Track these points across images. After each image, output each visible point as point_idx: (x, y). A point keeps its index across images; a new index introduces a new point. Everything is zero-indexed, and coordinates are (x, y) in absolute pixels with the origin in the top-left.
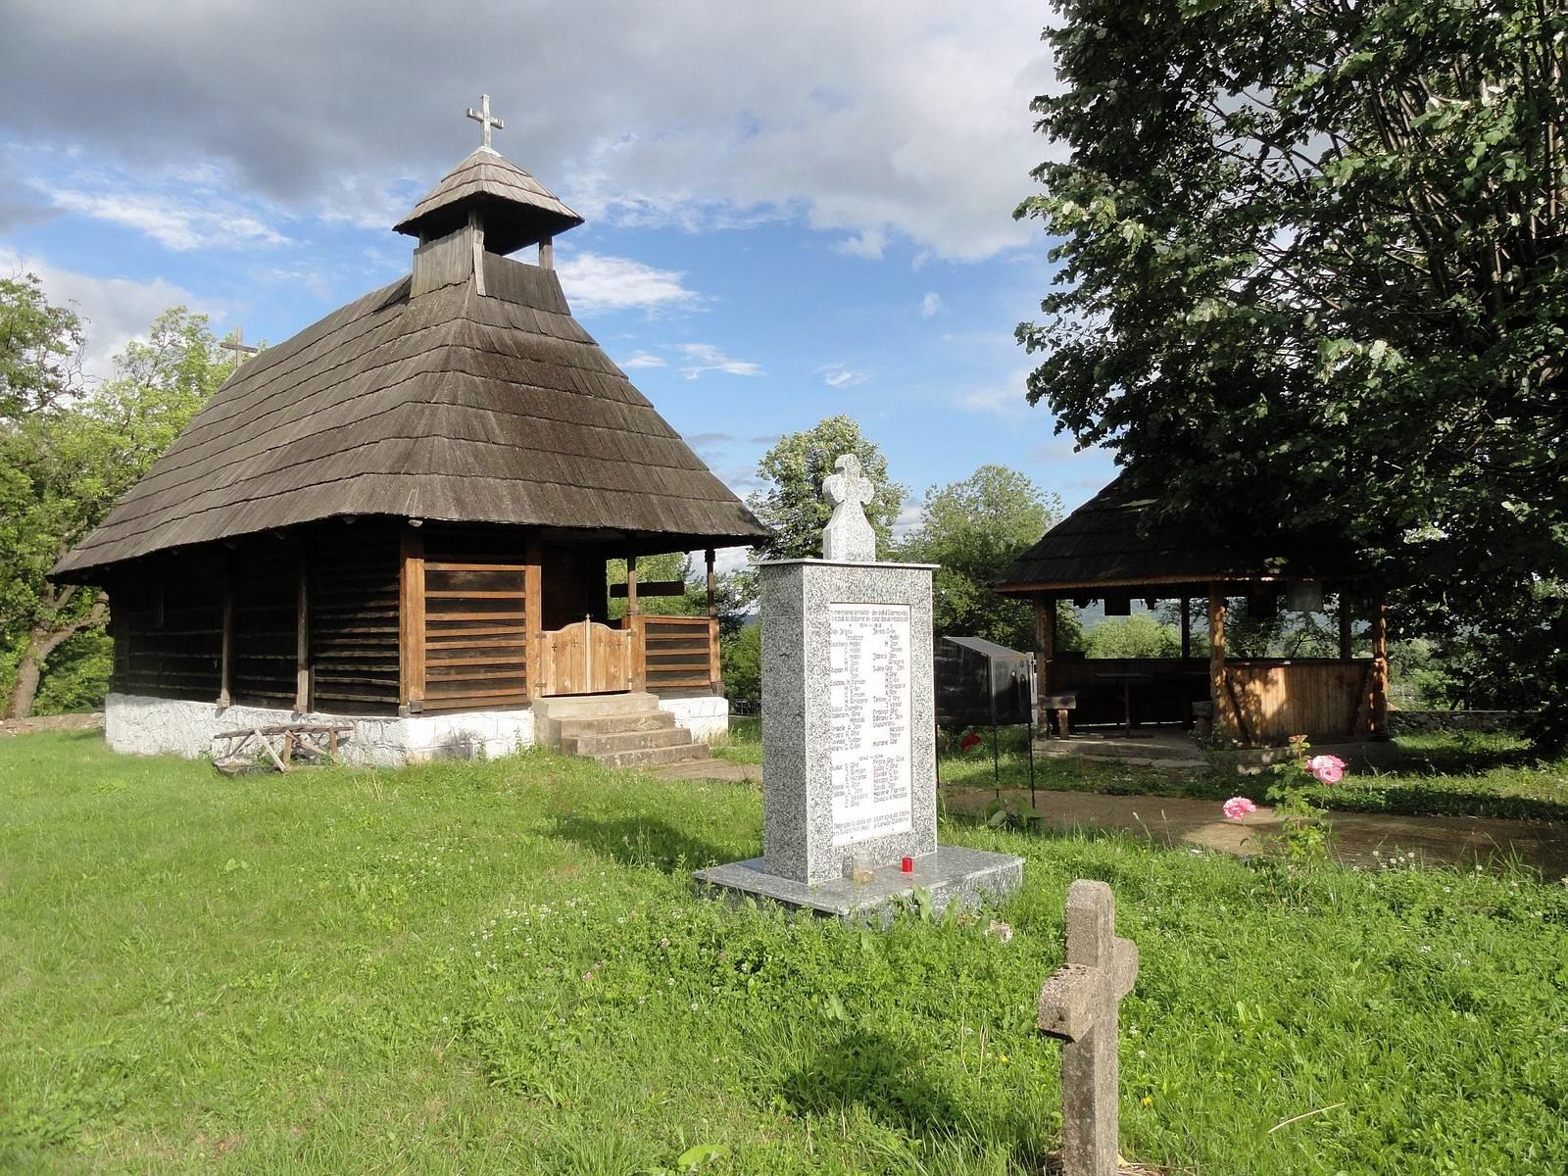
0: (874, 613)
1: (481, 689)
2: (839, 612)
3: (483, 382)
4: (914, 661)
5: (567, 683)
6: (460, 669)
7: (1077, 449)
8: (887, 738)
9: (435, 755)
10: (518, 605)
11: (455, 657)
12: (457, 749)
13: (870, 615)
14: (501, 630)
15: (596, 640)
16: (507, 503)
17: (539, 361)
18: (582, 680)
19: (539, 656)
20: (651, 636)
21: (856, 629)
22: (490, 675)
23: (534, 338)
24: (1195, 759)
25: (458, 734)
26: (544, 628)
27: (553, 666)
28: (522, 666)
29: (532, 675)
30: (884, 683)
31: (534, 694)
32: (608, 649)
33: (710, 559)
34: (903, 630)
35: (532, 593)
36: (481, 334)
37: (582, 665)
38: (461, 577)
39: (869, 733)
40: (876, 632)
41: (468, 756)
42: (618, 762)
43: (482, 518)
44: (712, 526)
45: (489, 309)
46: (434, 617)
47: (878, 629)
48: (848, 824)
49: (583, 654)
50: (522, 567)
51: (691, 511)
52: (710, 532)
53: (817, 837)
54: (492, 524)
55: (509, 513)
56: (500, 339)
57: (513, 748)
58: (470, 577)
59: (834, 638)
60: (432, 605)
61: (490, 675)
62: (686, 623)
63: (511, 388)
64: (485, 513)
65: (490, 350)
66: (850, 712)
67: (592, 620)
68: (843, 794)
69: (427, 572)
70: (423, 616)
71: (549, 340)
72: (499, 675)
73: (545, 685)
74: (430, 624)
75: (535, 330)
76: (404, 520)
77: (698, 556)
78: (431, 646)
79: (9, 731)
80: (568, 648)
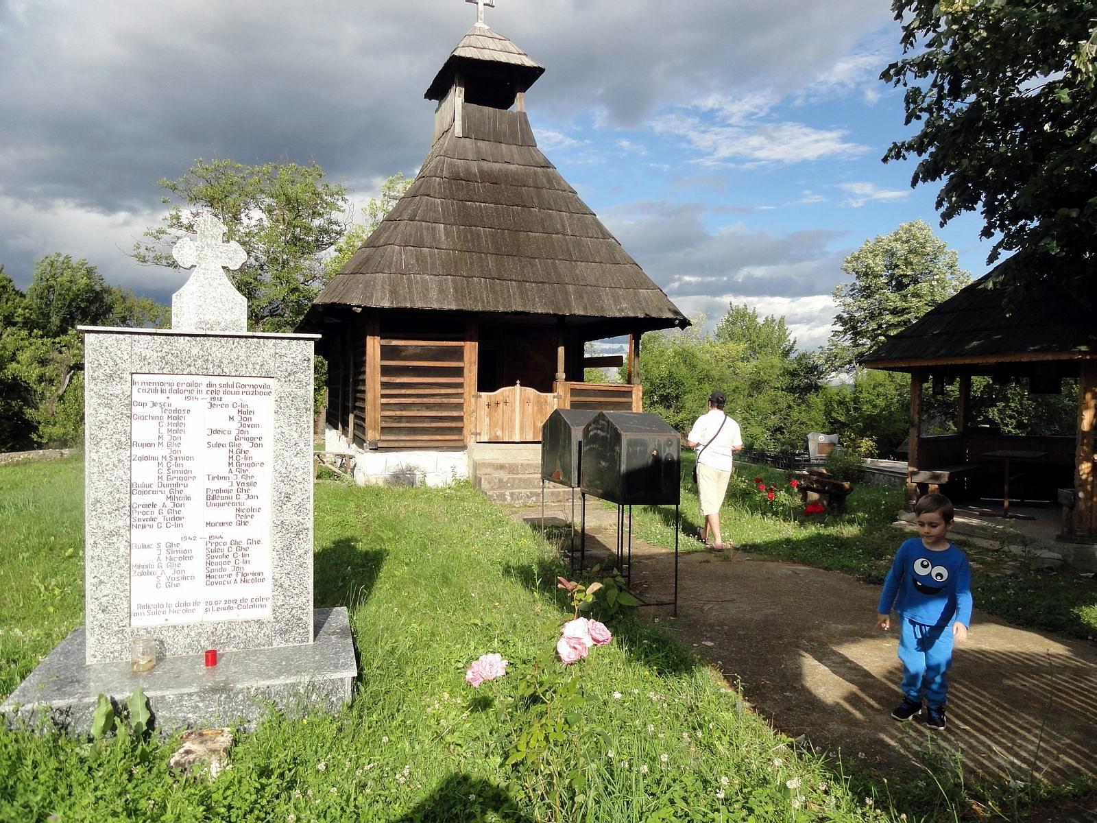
0: (209, 385)
1: (425, 434)
2: (149, 384)
3: (442, 203)
4: (281, 438)
5: (499, 433)
6: (410, 419)
7: (942, 225)
9: (386, 481)
10: (459, 372)
11: (405, 410)
12: (403, 479)
13: (204, 388)
14: (443, 391)
15: (525, 401)
16: (434, 294)
17: (496, 183)
18: (512, 432)
19: (474, 411)
20: (576, 399)
21: (178, 401)
22: (434, 425)
23: (497, 166)
24: (1049, 550)
25: (404, 467)
27: (487, 420)
28: (460, 419)
29: (468, 425)
31: (470, 441)
32: (536, 408)
34: (263, 408)
35: (470, 363)
36: (452, 166)
37: (512, 420)
38: (411, 351)
39: (196, 513)
40: (212, 406)
41: (412, 483)
42: (509, 498)
43: (409, 306)
44: (621, 310)
45: (464, 147)
46: (385, 379)
47: (217, 402)
48: (159, 606)
49: (513, 411)
50: (462, 343)
52: (617, 315)
53: (101, 616)
55: (433, 302)
56: (468, 171)
57: (449, 480)
58: (418, 350)
59: (136, 410)
60: (385, 371)
61: (434, 425)
62: (611, 389)
63: (464, 207)
64: (412, 301)
65: (456, 178)
66: (167, 490)
67: (522, 385)
68: (152, 574)
69: (382, 347)
70: (379, 378)
71: (512, 167)
72: (440, 425)
73: (480, 434)
74: (385, 385)
76: (348, 308)
78: (384, 401)
80: (500, 406)
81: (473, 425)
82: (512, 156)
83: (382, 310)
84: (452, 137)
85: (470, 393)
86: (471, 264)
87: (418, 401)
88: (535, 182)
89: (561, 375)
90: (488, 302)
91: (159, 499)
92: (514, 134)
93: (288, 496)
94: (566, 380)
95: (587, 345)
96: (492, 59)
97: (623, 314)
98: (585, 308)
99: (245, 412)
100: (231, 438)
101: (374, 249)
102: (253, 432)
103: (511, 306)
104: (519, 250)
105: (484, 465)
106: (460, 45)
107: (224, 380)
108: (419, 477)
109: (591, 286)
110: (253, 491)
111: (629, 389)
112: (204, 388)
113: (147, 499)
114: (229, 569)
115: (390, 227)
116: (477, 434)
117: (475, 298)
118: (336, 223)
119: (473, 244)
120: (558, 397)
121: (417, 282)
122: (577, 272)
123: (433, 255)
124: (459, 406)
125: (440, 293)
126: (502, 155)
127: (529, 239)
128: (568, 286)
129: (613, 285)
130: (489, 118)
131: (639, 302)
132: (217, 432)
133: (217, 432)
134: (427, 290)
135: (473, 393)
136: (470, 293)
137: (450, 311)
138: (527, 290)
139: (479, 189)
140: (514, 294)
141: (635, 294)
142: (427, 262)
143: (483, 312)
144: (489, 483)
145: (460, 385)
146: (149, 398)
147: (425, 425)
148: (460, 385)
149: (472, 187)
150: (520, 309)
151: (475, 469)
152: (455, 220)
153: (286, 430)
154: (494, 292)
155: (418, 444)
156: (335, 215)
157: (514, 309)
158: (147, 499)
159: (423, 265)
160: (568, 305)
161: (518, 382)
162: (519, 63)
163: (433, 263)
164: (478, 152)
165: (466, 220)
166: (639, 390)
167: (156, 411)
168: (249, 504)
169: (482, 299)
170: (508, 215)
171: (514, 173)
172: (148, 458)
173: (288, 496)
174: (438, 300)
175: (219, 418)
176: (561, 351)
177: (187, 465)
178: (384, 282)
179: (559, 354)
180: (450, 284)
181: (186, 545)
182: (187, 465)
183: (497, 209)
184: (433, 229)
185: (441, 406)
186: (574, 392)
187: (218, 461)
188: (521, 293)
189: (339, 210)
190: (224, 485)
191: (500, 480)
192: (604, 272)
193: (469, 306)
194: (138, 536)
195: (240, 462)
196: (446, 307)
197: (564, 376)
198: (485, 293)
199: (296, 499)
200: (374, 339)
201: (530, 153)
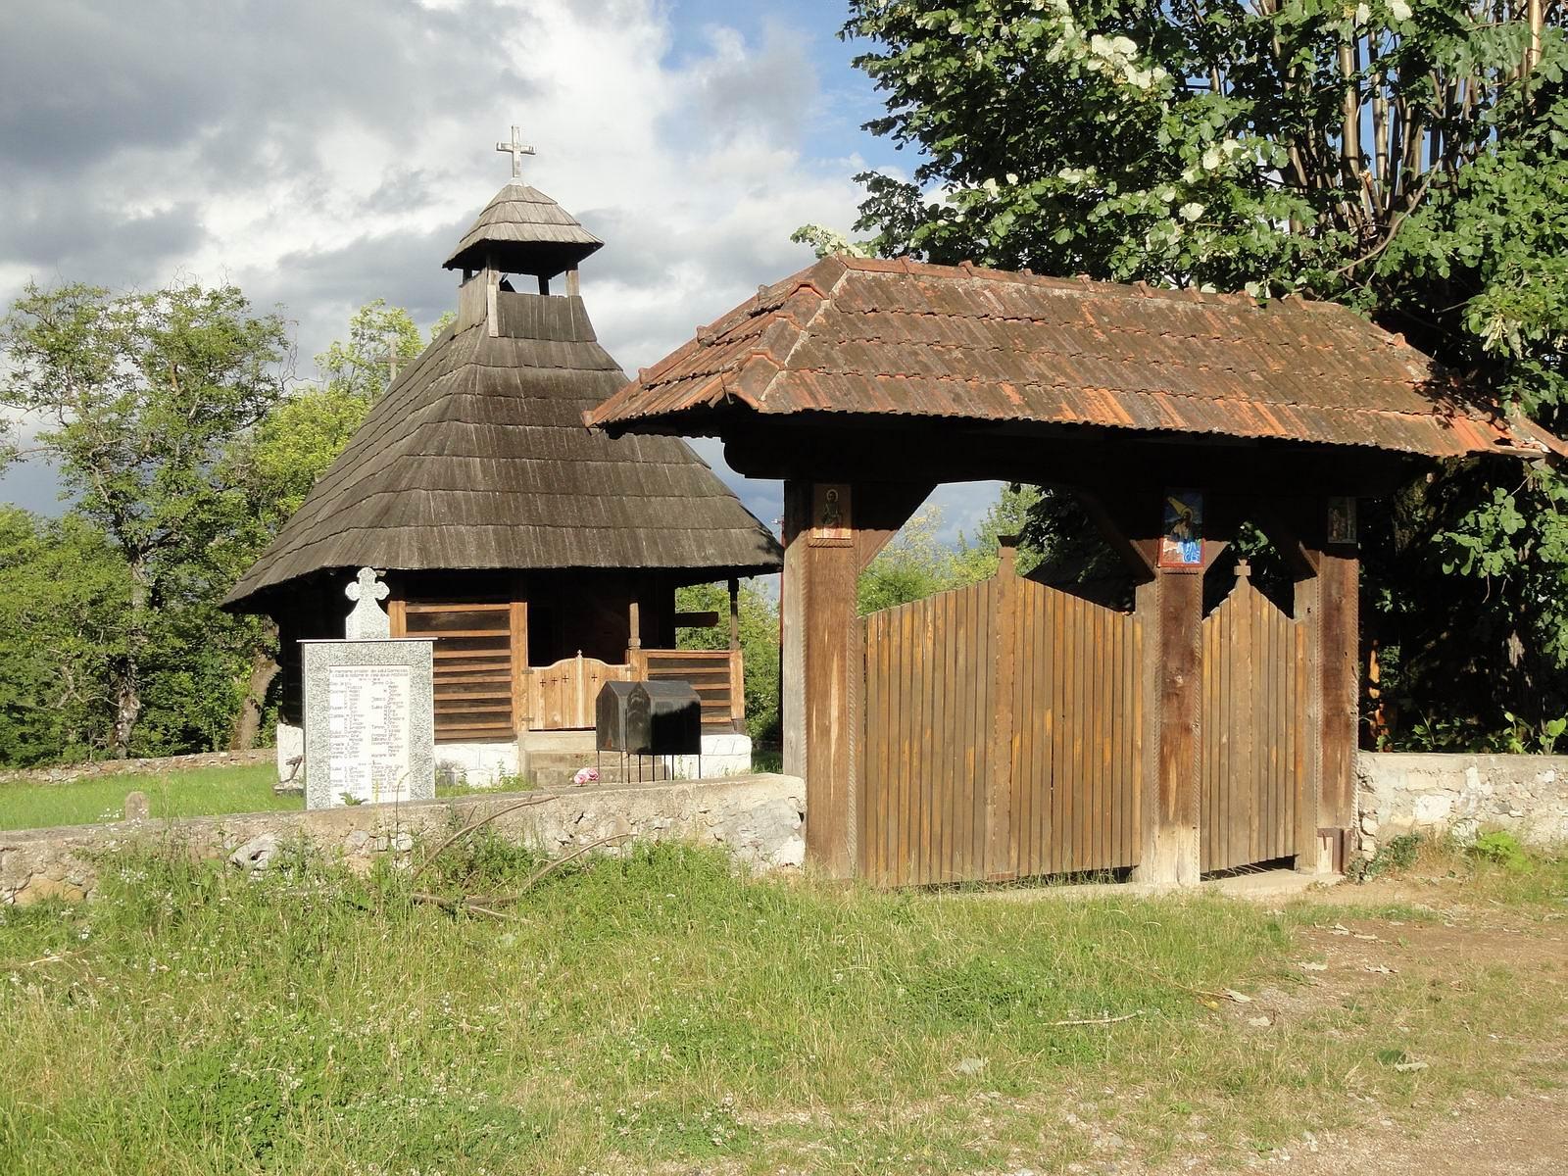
1: (464, 722)
3: (476, 429)
4: (415, 703)
5: (558, 718)
8: (387, 752)
10: (503, 643)
13: (369, 673)
14: (485, 667)
21: (355, 681)
22: (474, 710)
23: (546, 372)
25: (439, 763)
26: (531, 664)
27: (542, 702)
28: (507, 701)
29: (518, 709)
30: (383, 716)
31: (521, 729)
33: (734, 589)
34: (403, 683)
36: (486, 376)
37: (573, 701)
38: (443, 619)
39: (367, 749)
43: (442, 566)
44: (705, 558)
49: (575, 689)
50: (506, 606)
51: (684, 542)
52: (701, 564)
54: (453, 570)
56: (508, 385)
57: (496, 779)
58: (452, 618)
59: (332, 688)
61: (474, 710)
63: (505, 433)
64: (446, 560)
65: (491, 392)
71: (565, 373)
72: (483, 709)
73: (533, 720)
75: (560, 366)
77: (721, 587)
79: (233, 763)
80: (558, 683)
81: (523, 708)
82: (564, 357)
83: (411, 572)
84: (485, 336)
85: (519, 667)
86: (517, 508)
87: (454, 680)
88: (595, 390)
89: (635, 641)
90: (539, 556)
91: (345, 740)
92: (566, 325)
93: (419, 738)
94: (642, 647)
95: (679, 591)
96: (535, 239)
97: (709, 563)
98: (660, 558)
99: (393, 687)
100: (386, 703)
101: (395, 495)
102: (397, 699)
103: (566, 560)
104: (575, 485)
105: (541, 756)
106: (493, 221)
107: (380, 668)
108: (457, 775)
109: (668, 528)
110: (399, 735)
111: (726, 656)
112: (369, 673)
113: (338, 741)
114: (385, 784)
115: (412, 465)
116: (529, 720)
117: (523, 551)
118: (268, 381)
119: (518, 483)
120: (632, 669)
121: (451, 536)
122: (651, 511)
123: (468, 501)
124: (506, 686)
125: (479, 548)
126: (551, 356)
127: (588, 471)
128: (638, 531)
129: (697, 526)
130: (533, 308)
131: (730, 545)
132: (377, 699)
133: (377, 699)
134: (463, 544)
135: (522, 668)
136: (516, 546)
137: (492, 571)
138: (586, 538)
139: (522, 408)
140: (571, 544)
141: (725, 535)
142: (461, 510)
143: (533, 569)
144: (546, 777)
145: (507, 659)
146: (339, 680)
147: (464, 710)
148: (507, 659)
149: (513, 405)
150: (578, 563)
151: (528, 764)
152: (494, 452)
153: (417, 697)
154: (545, 543)
155: (455, 735)
156: (271, 370)
157: (571, 563)
158: (338, 741)
159: (455, 511)
160: (638, 554)
161: (580, 652)
162: (569, 239)
163: (468, 510)
164: (520, 355)
165: (506, 448)
166: (738, 657)
167: (343, 688)
168: (395, 743)
169: (531, 551)
170: (561, 439)
171: (568, 381)
172: (340, 716)
173: (419, 738)
174: (478, 557)
175: (379, 691)
176: (634, 608)
177: (361, 720)
178: (410, 539)
179: (632, 615)
180: (491, 535)
181: (360, 768)
182: (361, 720)
183: (546, 433)
184: (467, 465)
185: (482, 686)
186: (653, 663)
187: (378, 717)
188: (579, 542)
189: (273, 359)
190: (381, 731)
191: (560, 774)
192: (685, 507)
193: (515, 562)
194: (334, 763)
195: (390, 717)
196: (488, 566)
197: (639, 643)
198: (534, 544)
199: (424, 740)
200: (398, 606)
201: (588, 350)
